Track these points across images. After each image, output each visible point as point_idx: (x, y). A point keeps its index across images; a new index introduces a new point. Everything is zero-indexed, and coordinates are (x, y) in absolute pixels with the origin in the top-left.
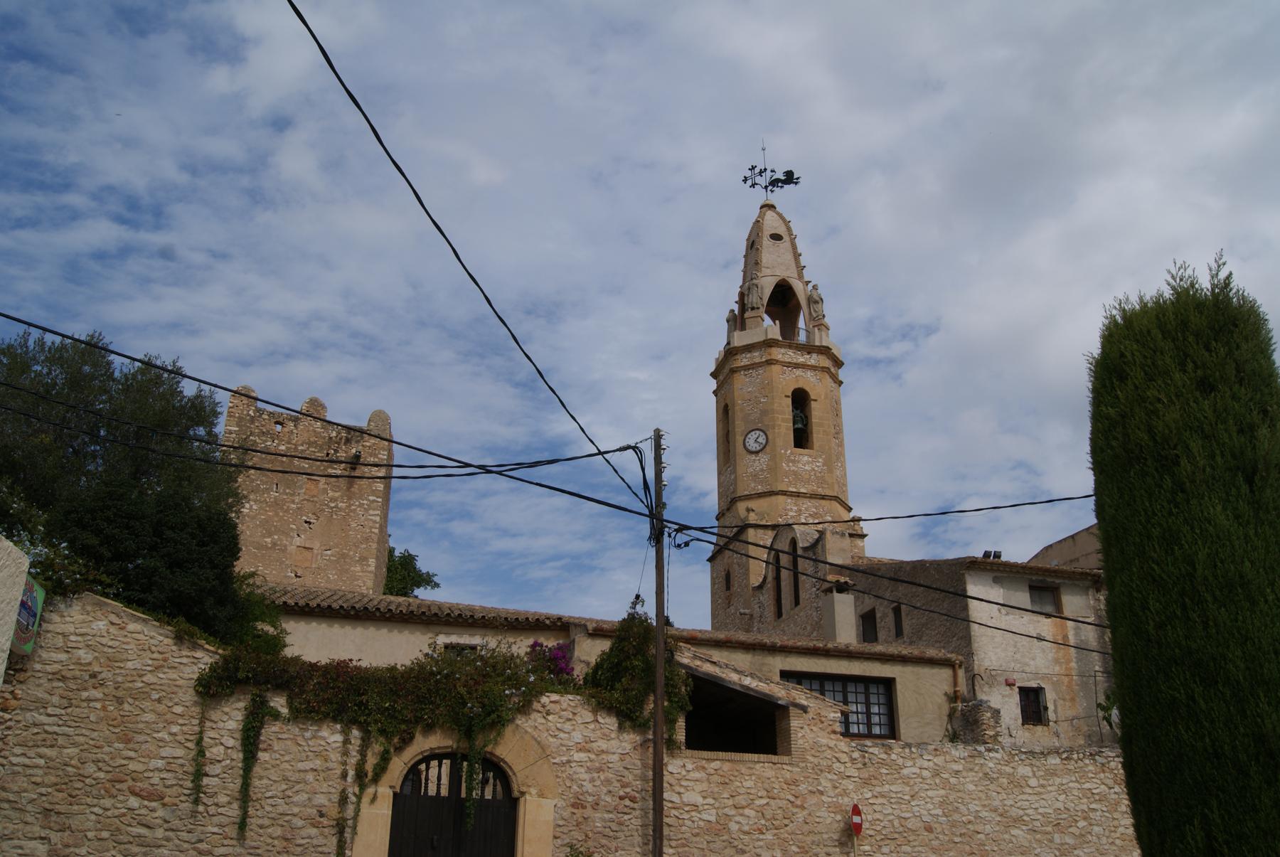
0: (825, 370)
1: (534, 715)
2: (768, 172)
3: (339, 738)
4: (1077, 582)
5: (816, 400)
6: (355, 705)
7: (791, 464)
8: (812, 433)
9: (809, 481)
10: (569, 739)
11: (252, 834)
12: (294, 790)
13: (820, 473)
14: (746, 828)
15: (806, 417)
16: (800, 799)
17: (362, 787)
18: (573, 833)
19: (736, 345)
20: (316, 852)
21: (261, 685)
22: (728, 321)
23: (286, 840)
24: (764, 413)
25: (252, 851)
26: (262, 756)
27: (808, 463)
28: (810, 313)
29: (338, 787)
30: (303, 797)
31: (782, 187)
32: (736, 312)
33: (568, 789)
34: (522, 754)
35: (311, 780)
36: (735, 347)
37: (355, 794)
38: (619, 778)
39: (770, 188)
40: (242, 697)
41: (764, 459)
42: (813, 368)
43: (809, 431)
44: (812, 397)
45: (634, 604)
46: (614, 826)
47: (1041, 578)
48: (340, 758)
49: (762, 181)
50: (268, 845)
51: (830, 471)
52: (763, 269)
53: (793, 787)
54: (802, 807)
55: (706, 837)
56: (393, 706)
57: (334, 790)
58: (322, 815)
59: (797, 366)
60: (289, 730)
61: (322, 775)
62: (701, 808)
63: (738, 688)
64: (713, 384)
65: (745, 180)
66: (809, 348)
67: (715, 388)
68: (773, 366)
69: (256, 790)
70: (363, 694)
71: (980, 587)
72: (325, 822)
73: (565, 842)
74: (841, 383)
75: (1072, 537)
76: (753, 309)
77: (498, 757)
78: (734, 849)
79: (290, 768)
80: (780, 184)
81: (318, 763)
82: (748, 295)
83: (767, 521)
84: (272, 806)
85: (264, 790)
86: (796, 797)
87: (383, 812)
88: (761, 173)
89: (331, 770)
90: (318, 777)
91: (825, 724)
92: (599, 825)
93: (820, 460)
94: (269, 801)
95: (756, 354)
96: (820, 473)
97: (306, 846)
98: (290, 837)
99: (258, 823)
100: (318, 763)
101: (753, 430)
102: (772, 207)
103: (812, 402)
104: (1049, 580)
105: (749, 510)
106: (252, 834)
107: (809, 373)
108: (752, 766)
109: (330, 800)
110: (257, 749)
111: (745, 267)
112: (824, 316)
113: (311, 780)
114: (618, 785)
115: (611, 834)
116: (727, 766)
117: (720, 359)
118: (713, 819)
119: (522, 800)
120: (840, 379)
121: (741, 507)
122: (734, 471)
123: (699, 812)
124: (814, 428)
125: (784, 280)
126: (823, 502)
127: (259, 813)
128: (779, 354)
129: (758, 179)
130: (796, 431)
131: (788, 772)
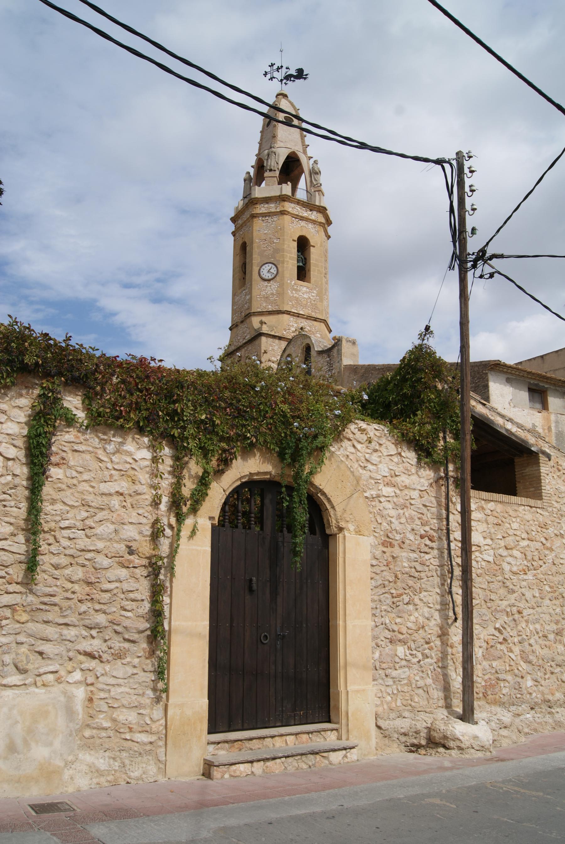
0: (320, 224)
1: (346, 443)
2: (284, 69)
3: (147, 454)
4: (558, 388)
5: (314, 246)
6: (167, 414)
7: (294, 292)
8: (309, 270)
9: (305, 306)
10: (377, 472)
11: (46, 577)
12: (97, 518)
13: (314, 301)
14: (515, 569)
15: (305, 259)
16: (549, 541)
17: (180, 518)
18: (384, 573)
19: (256, 196)
20: (127, 600)
21: (53, 377)
22: (245, 180)
23: (89, 584)
24: (277, 251)
25: (46, 599)
26: (54, 472)
27: (306, 292)
28: (311, 181)
29: (150, 517)
30: (106, 529)
31: (294, 81)
32: (252, 174)
33: (379, 526)
34: (340, 486)
35: (117, 507)
36: (257, 198)
37: (171, 527)
38: (420, 516)
39: (284, 81)
40: (24, 392)
41: (274, 285)
42: (314, 222)
43: (307, 269)
44: (312, 244)
45: (422, 336)
46: (419, 568)
47: (536, 382)
48: (149, 481)
49: (279, 75)
50: (67, 591)
51: (321, 300)
52: (278, 142)
53: (544, 530)
54: (551, 550)
55: (487, 577)
56: (211, 420)
57: (144, 521)
58: (131, 552)
59: (302, 218)
60: (86, 440)
61: (129, 500)
62: (483, 549)
63: (503, 432)
64: (232, 227)
65: (266, 74)
66: (310, 206)
67: (234, 230)
68: (285, 216)
69: (49, 518)
70: (174, 402)
71: (498, 384)
72: (137, 561)
73: (379, 583)
74: (329, 237)
75: (542, 357)
76: (271, 170)
77: (316, 487)
78: (507, 589)
79: (91, 490)
80: (292, 79)
81: (123, 485)
82: (267, 160)
83: (275, 332)
84: (70, 539)
85: (58, 518)
86: (546, 539)
87: (204, 548)
88: (278, 69)
89: (140, 494)
90: (124, 504)
91: (561, 472)
92: (406, 564)
93: (315, 292)
94: (66, 533)
95: (272, 205)
96: (314, 301)
97: (115, 592)
98: (93, 580)
99: (52, 562)
100: (123, 485)
101: (267, 263)
102: (285, 96)
103: (311, 248)
104: (541, 384)
105: (262, 323)
106: (46, 577)
107: (310, 226)
108: (517, 509)
109: (140, 533)
110: (49, 462)
111: (261, 140)
112: (321, 184)
113: (117, 507)
114: (420, 523)
115: (416, 574)
116: (499, 508)
117: (240, 208)
118: (491, 559)
119: (341, 536)
120: (329, 234)
121: (255, 321)
122: (250, 293)
123: (481, 553)
124: (312, 267)
125: (294, 153)
126: (315, 323)
127: (53, 548)
128: (289, 206)
129: (276, 74)
130: (299, 267)
131: (543, 516)
